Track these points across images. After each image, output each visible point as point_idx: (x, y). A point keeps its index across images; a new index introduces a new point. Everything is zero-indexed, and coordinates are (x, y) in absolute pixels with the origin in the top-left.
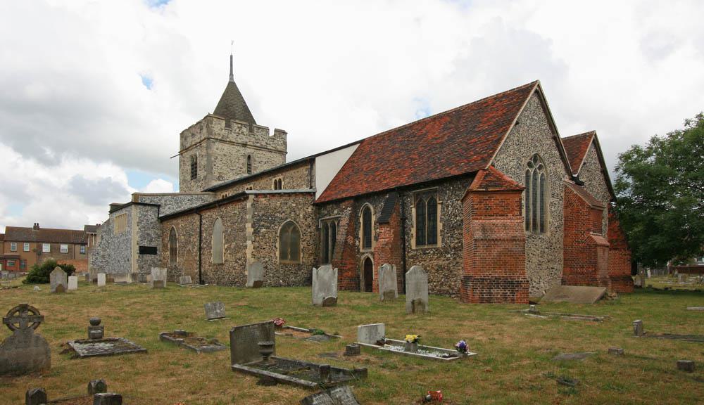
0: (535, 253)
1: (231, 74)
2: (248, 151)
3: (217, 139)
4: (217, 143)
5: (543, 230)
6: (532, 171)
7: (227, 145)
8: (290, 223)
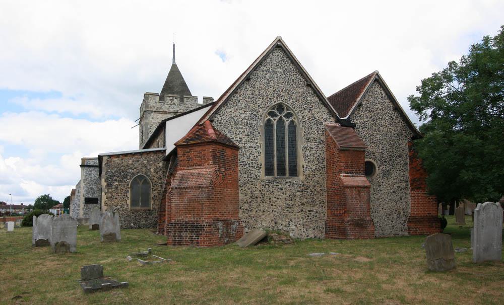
0: (280, 197)
1: (174, 58)
4: (152, 114)
5: (294, 172)
6: (275, 121)
8: (140, 177)
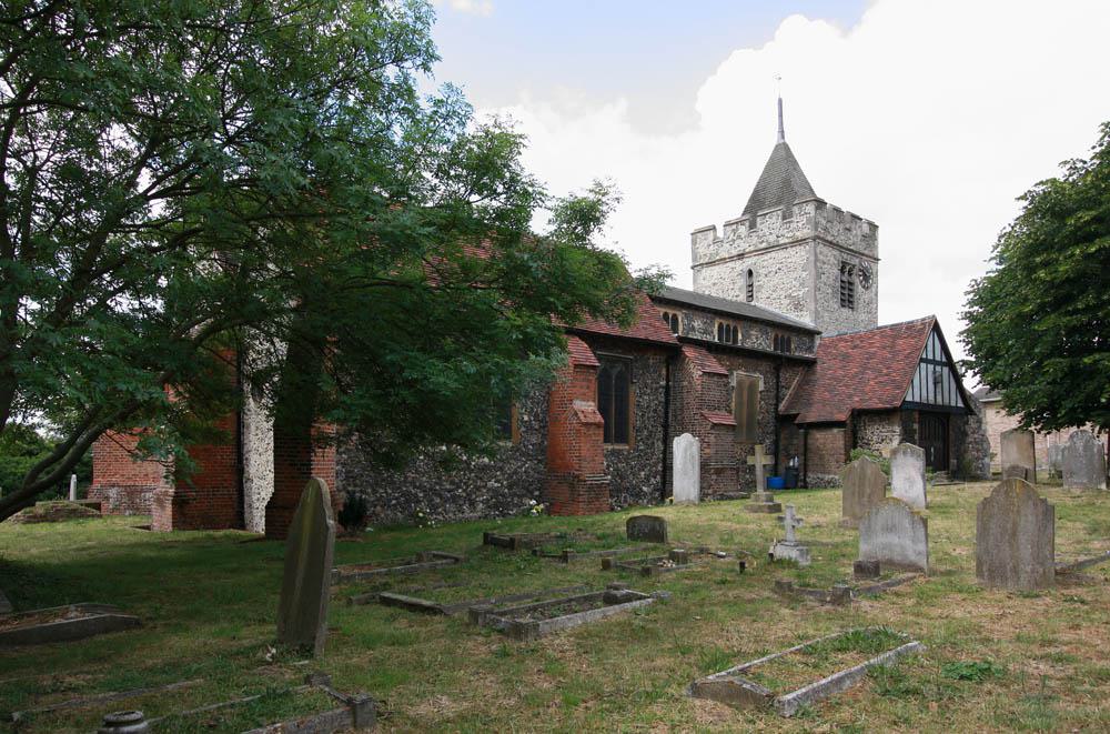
1: (782, 132)
2: (748, 262)
3: (702, 264)
7: (717, 267)
